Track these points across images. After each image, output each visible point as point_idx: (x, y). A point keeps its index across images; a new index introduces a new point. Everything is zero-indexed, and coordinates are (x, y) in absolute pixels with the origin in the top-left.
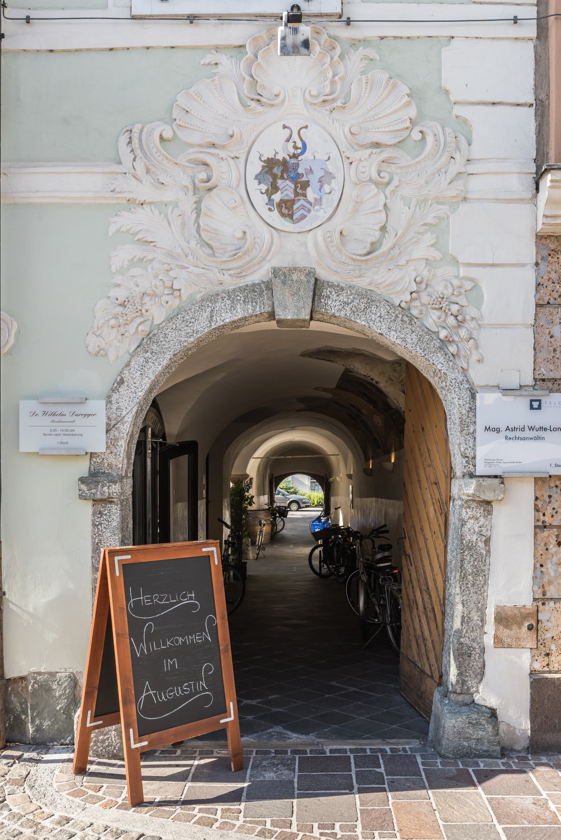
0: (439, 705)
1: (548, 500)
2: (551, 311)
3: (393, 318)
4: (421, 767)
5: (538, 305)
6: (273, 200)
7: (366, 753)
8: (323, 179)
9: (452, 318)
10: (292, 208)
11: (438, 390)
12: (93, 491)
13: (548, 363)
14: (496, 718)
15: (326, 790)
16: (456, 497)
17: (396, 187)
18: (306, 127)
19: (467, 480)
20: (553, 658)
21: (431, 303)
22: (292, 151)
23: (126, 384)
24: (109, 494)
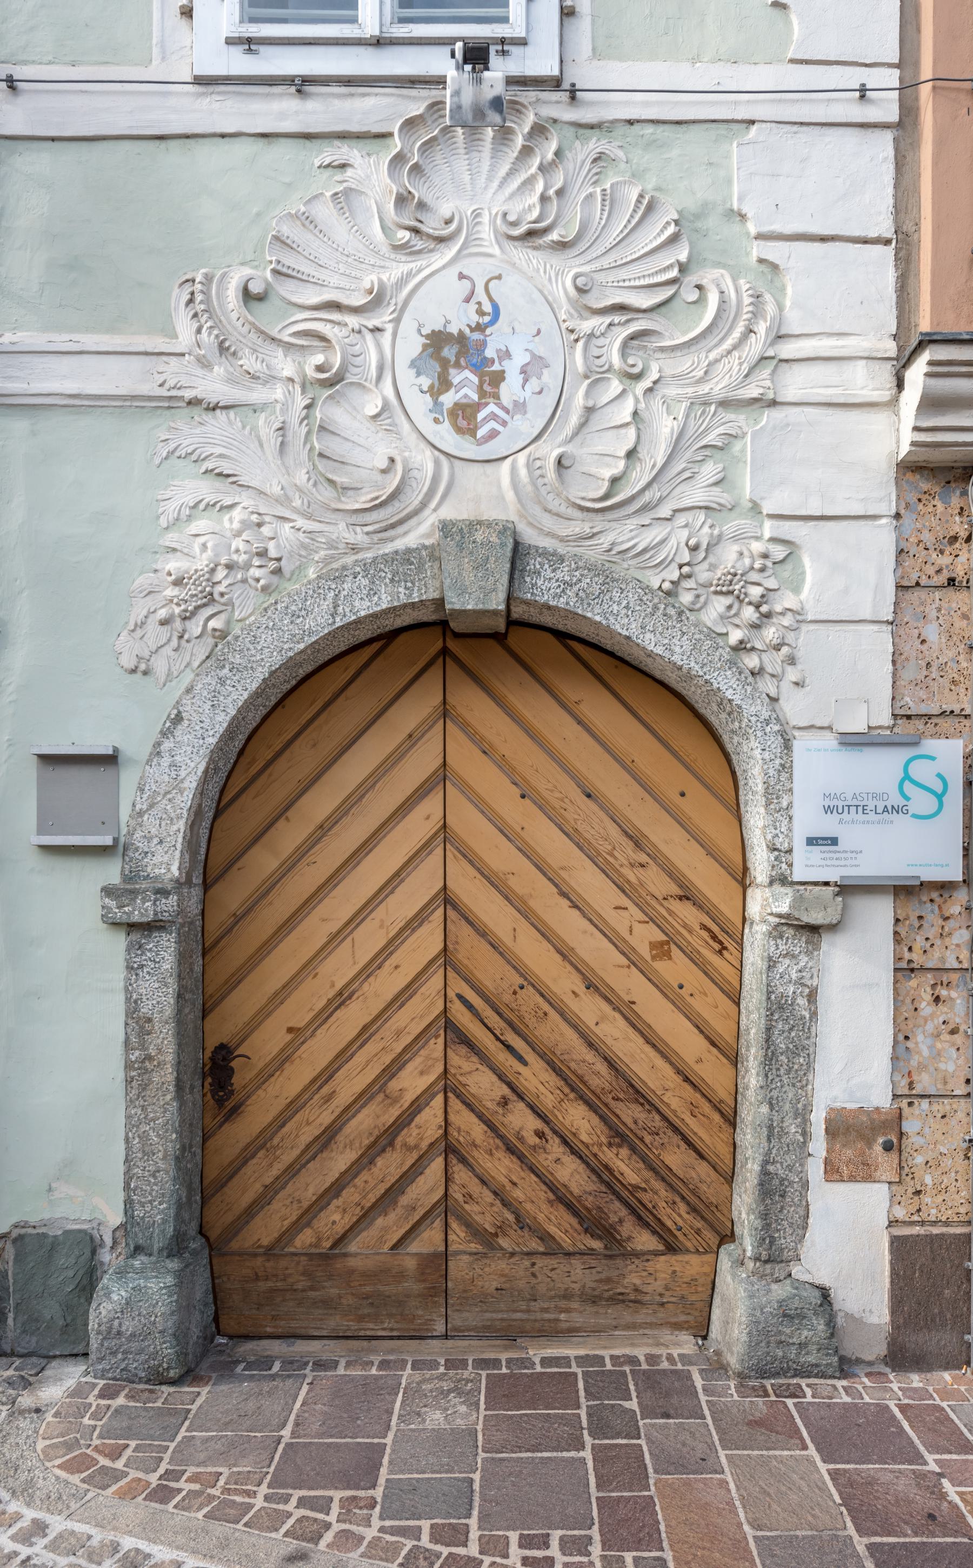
0: (729, 1279)
1: (917, 924)
2: (923, 597)
3: (649, 610)
4: (703, 1398)
5: (900, 587)
6: (442, 404)
7: (605, 1366)
8: (529, 368)
9: (751, 609)
10: (475, 418)
11: (724, 736)
12: (126, 909)
13: (918, 688)
14: (830, 1304)
15: (533, 1451)
16: (757, 918)
17: (655, 383)
18: (499, 277)
19: (777, 888)
20: (927, 1199)
21: (715, 582)
22: (474, 318)
23: (186, 723)
24: (156, 914)
